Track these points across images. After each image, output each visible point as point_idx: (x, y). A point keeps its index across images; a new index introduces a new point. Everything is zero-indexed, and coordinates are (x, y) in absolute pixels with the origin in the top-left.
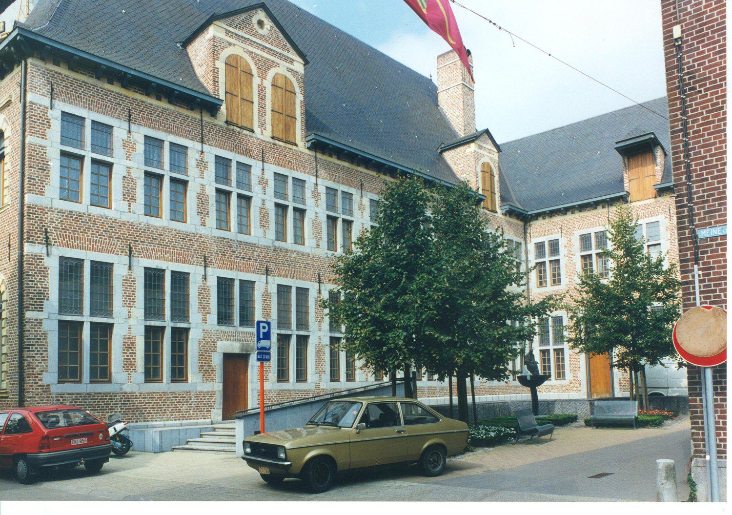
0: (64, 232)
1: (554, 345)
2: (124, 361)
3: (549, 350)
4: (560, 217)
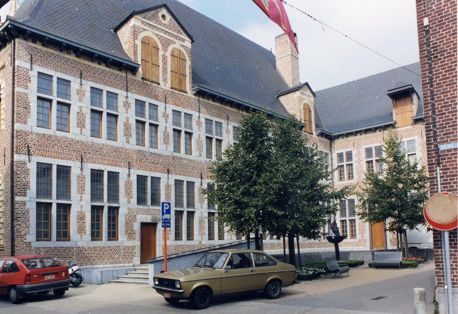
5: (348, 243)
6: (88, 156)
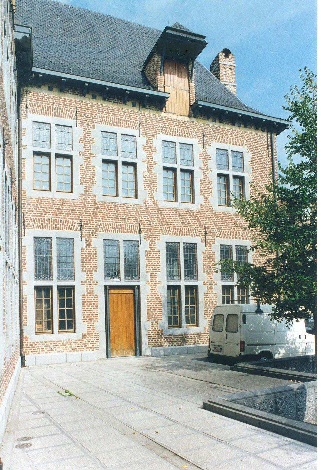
0: (215, 134)
1: (59, 279)
2: (147, 156)
3: (51, 287)
4: (71, 95)
5: (55, 345)
6: (29, 217)
